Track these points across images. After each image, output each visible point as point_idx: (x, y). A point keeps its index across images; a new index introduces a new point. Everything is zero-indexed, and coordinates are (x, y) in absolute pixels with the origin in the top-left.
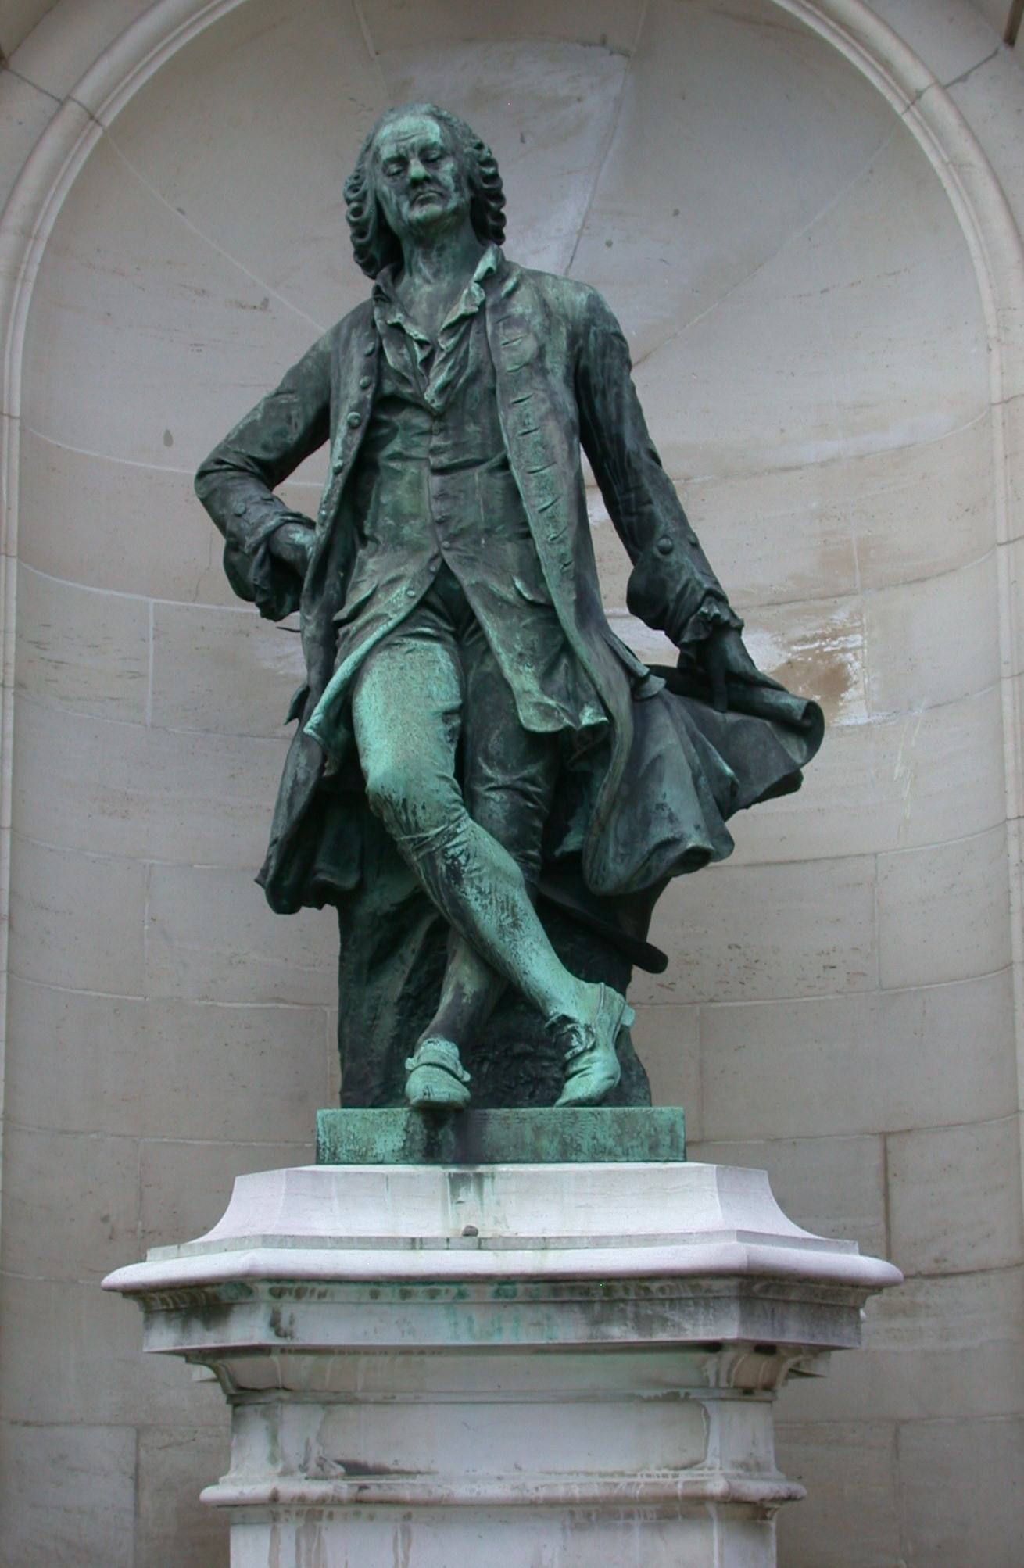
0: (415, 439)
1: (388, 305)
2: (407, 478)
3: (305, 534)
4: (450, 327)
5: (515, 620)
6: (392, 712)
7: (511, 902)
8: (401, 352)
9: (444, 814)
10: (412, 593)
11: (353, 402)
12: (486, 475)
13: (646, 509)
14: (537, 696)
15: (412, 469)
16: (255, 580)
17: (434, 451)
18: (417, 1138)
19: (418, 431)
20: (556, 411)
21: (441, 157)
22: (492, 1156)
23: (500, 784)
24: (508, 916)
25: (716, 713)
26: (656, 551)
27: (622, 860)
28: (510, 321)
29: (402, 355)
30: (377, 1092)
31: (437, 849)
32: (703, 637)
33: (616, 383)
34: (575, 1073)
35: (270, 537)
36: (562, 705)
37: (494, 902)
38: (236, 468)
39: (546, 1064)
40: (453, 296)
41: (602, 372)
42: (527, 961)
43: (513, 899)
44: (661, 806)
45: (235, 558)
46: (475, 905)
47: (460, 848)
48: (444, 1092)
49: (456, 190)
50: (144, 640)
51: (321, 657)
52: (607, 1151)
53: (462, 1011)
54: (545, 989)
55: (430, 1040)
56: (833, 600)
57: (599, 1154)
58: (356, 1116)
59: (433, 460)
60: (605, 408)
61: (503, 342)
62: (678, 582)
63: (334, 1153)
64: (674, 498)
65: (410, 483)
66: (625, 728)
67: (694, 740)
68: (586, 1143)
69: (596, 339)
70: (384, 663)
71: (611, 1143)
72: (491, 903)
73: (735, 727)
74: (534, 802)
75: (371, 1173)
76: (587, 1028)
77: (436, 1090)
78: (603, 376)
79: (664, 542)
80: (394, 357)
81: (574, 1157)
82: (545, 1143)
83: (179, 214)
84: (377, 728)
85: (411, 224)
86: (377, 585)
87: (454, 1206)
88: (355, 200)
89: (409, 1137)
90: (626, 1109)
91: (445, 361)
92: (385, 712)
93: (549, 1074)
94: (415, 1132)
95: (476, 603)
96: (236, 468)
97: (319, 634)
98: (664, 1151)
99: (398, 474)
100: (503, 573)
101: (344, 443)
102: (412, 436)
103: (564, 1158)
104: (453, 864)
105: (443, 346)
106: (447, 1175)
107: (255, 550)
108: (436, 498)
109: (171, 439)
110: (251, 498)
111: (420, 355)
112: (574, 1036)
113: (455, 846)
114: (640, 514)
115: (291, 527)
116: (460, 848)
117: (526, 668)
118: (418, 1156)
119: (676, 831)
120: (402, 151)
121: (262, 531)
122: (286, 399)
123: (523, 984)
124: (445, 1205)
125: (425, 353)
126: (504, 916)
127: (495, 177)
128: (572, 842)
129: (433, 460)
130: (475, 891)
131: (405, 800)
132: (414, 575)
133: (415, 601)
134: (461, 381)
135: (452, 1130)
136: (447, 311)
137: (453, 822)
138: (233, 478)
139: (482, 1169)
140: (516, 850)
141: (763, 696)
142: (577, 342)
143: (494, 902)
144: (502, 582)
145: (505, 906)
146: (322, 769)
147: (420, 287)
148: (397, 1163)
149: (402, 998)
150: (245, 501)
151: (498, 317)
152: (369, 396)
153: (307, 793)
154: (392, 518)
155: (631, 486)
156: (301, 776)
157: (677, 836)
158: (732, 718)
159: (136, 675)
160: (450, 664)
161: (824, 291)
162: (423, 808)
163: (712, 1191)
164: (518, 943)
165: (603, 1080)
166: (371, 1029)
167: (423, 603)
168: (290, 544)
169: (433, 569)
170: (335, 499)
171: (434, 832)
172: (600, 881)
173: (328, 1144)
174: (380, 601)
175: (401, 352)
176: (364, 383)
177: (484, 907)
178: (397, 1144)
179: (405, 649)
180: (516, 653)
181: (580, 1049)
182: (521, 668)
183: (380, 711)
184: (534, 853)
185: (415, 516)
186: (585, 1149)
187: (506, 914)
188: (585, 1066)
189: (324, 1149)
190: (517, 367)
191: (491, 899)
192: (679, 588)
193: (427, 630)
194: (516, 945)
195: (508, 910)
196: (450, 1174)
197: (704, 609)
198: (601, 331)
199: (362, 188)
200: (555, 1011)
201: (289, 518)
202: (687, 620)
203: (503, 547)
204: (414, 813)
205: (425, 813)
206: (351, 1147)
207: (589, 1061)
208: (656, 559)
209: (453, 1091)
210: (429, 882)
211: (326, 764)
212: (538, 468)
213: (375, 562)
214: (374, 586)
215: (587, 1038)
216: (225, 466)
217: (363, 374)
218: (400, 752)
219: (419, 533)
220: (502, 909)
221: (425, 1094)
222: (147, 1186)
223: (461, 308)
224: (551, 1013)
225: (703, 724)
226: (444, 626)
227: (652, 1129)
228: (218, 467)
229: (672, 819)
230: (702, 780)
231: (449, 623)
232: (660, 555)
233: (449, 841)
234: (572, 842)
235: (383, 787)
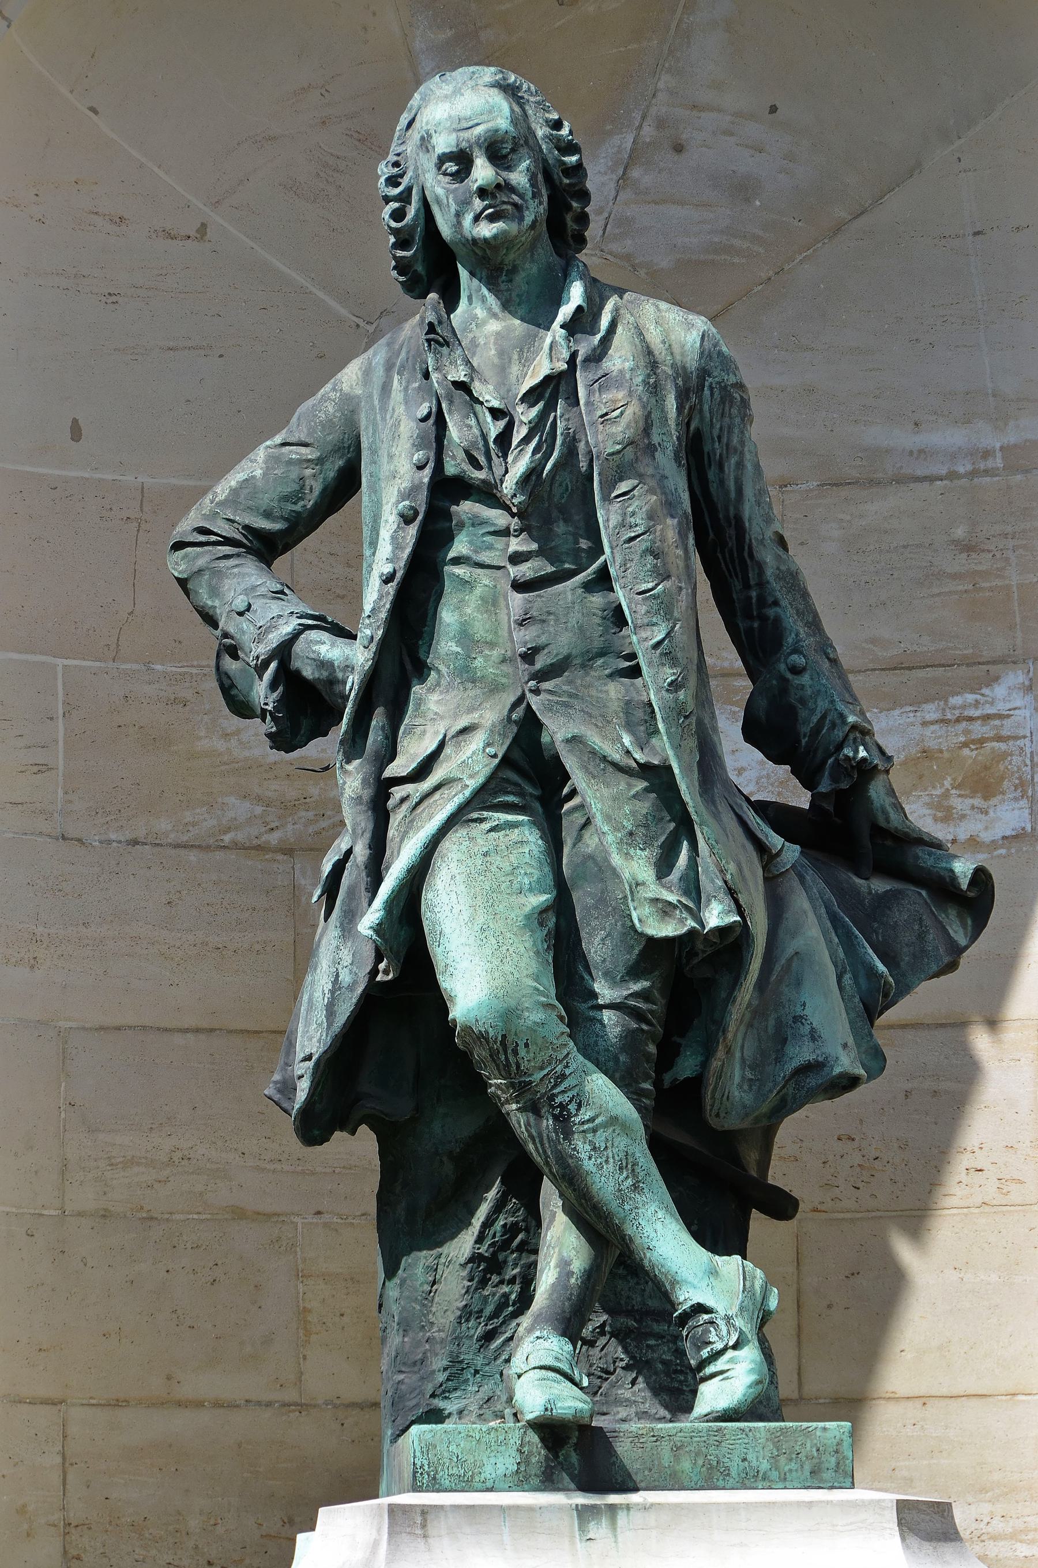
0: (489, 539)
1: (445, 350)
2: (478, 591)
3: (333, 645)
4: (532, 391)
5: (623, 786)
6: (481, 920)
7: (630, 1160)
8: (468, 422)
9: (551, 1052)
10: (491, 750)
11: (404, 483)
12: (580, 591)
13: (771, 612)
14: (654, 890)
15: (485, 578)
16: (266, 704)
17: (516, 559)
18: (534, 1460)
19: (492, 529)
20: (670, 505)
21: (513, 150)
22: (623, 1482)
23: (608, 1001)
24: (627, 1178)
25: (858, 881)
26: (782, 667)
27: (750, 1086)
28: (604, 382)
29: (470, 427)
30: (441, 1377)
31: (543, 1096)
32: (845, 785)
33: (736, 450)
34: (713, 1376)
35: (284, 651)
36: (684, 900)
37: (611, 1160)
38: (228, 541)
39: (652, 1342)
40: (526, 349)
41: (719, 437)
42: (653, 1235)
43: (633, 1154)
44: (798, 1019)
45: (230, 665)
46: (589, 1165)
47: (570, 1094)
48: (570, 1408)
49: (534, 197)
50: (51, 719)
51: (370, 826)
52: (760, 1475)
53: (571, 1294)
54: (674, 1269)
55: (538, 1333)
56: (985, 667)
57: (750, 1479)
58: (460, 1433)
59: (514, 571)
60: (722, 482)
61: (600, 413)
62: (813, 711)
63: (434, 1478)
64: (805, 595)
65: (482, 598)
66: (759, 926)
67: (834, 919)
68: (735, 1466)
69: (712, 395)
70: (463, 848)
71: (765, 1466)
72: (607, 1161)
73: (884, 901)
74: (648, 1023)
75: (483, 1507)
76: (728, 1319)
77: (559, 1405)
78: (719, 442)
79: (797, 659)
80: (460, 430)
81: (721, 1483)
82: (686, 1465)
83: (91, 114)
84: (463, 940)
85: (475, 241)
86: (445, 736)
87: (584, 1544)
88: (395, 199)
89: (525, 1459)
90: (782, 1424)
91: (526, 440)
92: (472, 919)
93: (655, 1355)
94: (530, 1453)
95: (570, 762)
96: (228, 541)
97: (367, 794)
98: (827, 1475)
99: (466, 584)
100: (602, 722)
101: (394, 538)
102: (483, 535)
103: (708, 1484)
104: (561, 1114)
105: (524, 419)
106: (574, 1506)
107: (266, 664)
108: (521, 623)
109: (80, 430)
110: (254, 588)
111: (494, 429)
112: (712, 1329)
113: (563, 1092)
114: (763, 618)
115: (313, 635)
116: (570, 1094)
117: (639, 852)
118: (535, 1481)
119: (818, 1052)
120: (464, 145)
121: (274, 639)
122: (297, 453)
123: (646, 1263)
124: (572, 1543)
125: (502, 424)
126: (622, 1178)
127: (579, 166)
128: (686, 1066)
129: (514, 571)
130: (588, 1147)
131: (504, 1037)
132: (493, 725)
133: (497, 761)
134: (549, 466)
135: (575, 1450)
136: (526, 362)
137: (561, 1061)
138: (227, 557)
139: (613, 1499)
140: (626, 1086)
141: (917, 857)
142: (688, 398)
143: (611, 1160)
144: (604, 737)
145: (624, 1164)
146: (374, 972)
147: (484, 322)
148: (510, 1489)
149: (471, 1260)
150: (246, 592)
151: (592, 376)
152: (426, 480)
153: (354, 1001)
154: (459, 643)
155: (752, 582)
156: (345, 978)
157: (820, 1059)
158: (880, 885)
159: (43, 768)
160: (540, 842)
161: (977, 234)
162: (527, 1045)
163: (891, 1529)
164: (640, 1211)
165: (750, 1387)
166: (429, 1296)
167: (506, 761)
168: (315, 660)
169: (514, 716)
170: (383, 615)
171: (538, 1076)
172: (722, 1115)
173: (426, 1468)
174: (449, 757)
175: (468, 422)
176: (419, 460)
177: (600, 1167)
178: (510, 1468)
179: (486, 826)
180: (624, 832)
181: (719, 1346)
182: (632, 851)
183: (466, 915)
184: (647, 1086)
185: (492, 645)
186: (734, 1472)
187: (625, 1174)
188: (726, 1368)
189: (422, 1474)
190: (619, 447)
191: (608, 1157)
192: (815, 719)
193: (511, 798)
194: (637, 1214)
195: (627, 1170)
196: (577, 1505)
197: (848, 752)
198: (719, 383)
199: (405, 182)
200: (687, 1296)
201: (310, 622)
202: (824, 762)
203: (605, 688)
204: (515, 1052)
205: (528, 1052)
206: (455, 1471)
207: (731, 1360)
208: (784, 680)
209: (580, 1405)
210: (531, 1136)
211: (382, 966)
212: (650, 585)
213: (438, 702)
214: (441, 737)
215: (729, 1332)
216: (213, 538)
217: (418, 446)
218: (497, 974)
219: (498, 668)
220: (621, 1168)
221: (546, 1409)
222: (72, 1464)
223: (542, 368)
224: (682, 1299)
225: (847, 898)
226: (529, 789)
227: (814, 1450)
228: (202, 538)
229: (814, 1036)
230: (847, 979)
231: (534, 785)
232: (789, 676)
233: (556, 1086)
234: (686, 1066)
235: (477, 1020)
